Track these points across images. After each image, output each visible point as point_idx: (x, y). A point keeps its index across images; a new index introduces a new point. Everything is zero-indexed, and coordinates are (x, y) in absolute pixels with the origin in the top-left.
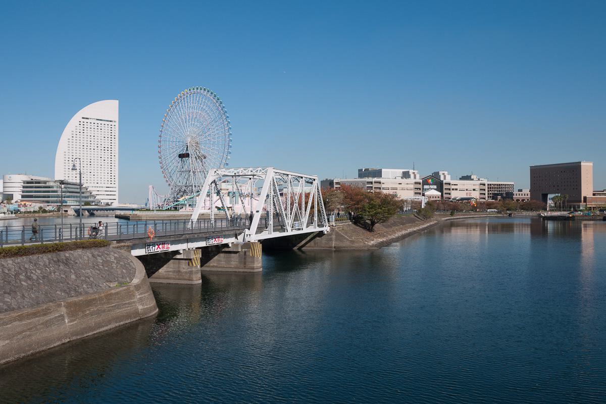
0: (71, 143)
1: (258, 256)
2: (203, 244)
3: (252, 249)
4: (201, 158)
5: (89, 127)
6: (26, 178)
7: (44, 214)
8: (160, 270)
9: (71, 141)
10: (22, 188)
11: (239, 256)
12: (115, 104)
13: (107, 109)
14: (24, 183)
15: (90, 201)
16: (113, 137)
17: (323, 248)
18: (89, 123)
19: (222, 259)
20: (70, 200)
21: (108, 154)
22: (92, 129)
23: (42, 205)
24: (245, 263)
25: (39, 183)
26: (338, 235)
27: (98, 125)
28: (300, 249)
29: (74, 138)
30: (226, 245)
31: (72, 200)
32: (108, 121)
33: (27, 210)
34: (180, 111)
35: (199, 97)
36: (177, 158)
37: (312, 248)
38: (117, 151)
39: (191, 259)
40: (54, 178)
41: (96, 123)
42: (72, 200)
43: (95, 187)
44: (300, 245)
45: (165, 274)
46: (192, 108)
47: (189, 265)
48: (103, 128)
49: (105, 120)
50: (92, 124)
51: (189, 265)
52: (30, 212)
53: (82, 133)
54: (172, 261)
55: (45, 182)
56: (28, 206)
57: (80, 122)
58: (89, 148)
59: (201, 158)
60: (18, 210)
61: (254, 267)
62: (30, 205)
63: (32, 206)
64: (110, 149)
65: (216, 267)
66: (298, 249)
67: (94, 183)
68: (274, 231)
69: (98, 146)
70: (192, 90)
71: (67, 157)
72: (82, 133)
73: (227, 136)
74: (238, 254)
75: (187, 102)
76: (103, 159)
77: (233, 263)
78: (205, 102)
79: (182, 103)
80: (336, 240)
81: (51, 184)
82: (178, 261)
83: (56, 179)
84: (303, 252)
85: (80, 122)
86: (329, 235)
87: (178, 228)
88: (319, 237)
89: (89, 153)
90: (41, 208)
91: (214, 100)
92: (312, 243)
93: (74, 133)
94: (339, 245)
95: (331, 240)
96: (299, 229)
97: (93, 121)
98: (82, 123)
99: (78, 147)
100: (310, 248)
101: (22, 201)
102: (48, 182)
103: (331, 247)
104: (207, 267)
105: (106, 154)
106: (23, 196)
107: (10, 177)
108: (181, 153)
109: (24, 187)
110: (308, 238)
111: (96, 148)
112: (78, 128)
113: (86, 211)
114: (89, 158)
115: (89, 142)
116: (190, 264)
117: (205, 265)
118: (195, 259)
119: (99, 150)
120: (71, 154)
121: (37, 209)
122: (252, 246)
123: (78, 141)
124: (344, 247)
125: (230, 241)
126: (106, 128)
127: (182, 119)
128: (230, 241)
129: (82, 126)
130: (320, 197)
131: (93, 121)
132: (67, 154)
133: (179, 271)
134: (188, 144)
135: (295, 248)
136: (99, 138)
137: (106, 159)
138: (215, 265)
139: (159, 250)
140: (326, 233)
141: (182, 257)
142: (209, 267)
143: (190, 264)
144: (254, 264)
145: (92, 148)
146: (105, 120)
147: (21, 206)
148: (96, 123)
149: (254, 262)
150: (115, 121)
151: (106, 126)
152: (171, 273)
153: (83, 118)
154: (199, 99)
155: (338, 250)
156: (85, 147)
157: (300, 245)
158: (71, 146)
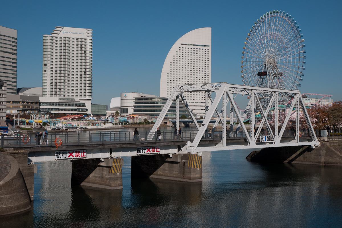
0: (172, 66)
1: (196, 167)
2: (135, 153)
3: (190, 160)
4: (278, 75)
5: (187, 51)
6: (137, 96)
7: (147, 125)
8: (90, 176)
9: (172, 64)
10: (134, 104)
11: (180, 166)
12: (90, 31)
13: (202, 36)
14: (136, 100)
15: (187, 115)
16: (207, 59)
17: (312, 163)
18: (187, 48)
19: (167, 168)
20: (170, 114)
21: (202, 74)
22: (190, 54)
23: (146, 117)
24: (184, 173)
25: (147, 99)
26: (328, 150)
27: (194, 50)
28: (290, 163)
29: (175, 62)
30: (167, 156)
31: (172, 114)
32: (202, 46)
33: (134, 121)
34: (260, 34)
35: (276, 20)
36: (257, 77)
37: (302, 163)
38: (210, 72)
39: (110, 167)
40: (159, 96)
41: (193, 48)
42: (172, 114)
43: (192, 103)
44: (291, 158)
45: (93, 179)
46: (270, 30)
47: (109, 172)
48: (198, 52)
49: (200, 46)
50: (190, 49)
51: (109, 172)
52: (137, 123)
53: (181, 57)
54: (98, 168)
55: (151, 99)
56: (135, 118)
57: (180, 48)
58: (187, 69)
59: (278, 75)
60: (127, 121)
61: (191, 177)
62: (137, 118)
63: (138, 118)
64: (204, 70)
65: (162, 175)
66: (288, 163)
67: (191, 99)
68: (227, 145)
69: (194, 67)
70: (269, 14)
71: (169, 77)
72: (181, 57)
73: (301, 54)
74: (179, 164)
75: (266, 25)
76: (198, 78)
77: (174, 172)
78: (281, 24)
79: (261, 27)
80: (326, 155)
81: (156, 100)
82: (102, 168)
83: (160, 97)
84: (292, 166)
85: (180, 48)
86: (318, 149)
87: (103, 138)
88: (309, 151)
89: (187, 74)
90: (145, 120)
91: (289, 22)
92: (302, 157)
93: (175, 57)
94: (329, 161)
95: (320, 154)
96: (272, 143)
97: (190, 47)
98: (181, 49)
99: (178, 69)
100: (299, 163)
101: (134, 114)
102: (154, 98)
103: (320, 162)
104: (155, 175)
105: (201, 74)
106: (135, 111)
107: (126, 95)
108: (260, 71)
109: (136, 103)
110: (298, 152)
111: (193, 69)
112: (178, 53)
113: (182, 123)
114: (187, 78)
115: (187, 64)
116: (110, 171)
117: (154, 173)
118: (114, 167)
119: (195, 71)
120: (172, 75)
121: (142, 120)
122: (189, 158)
123: (178, 64)
124: (334, 163)
125: (171, 152)
126: (201, 52)
127: (261, 41)
128: (171, 152)
129: (181, 51)
130: (305, 114)
131: (190, 47)
132: (169, 75)
133: (102, 177)
134: (267, 63)
135: (286, 161)
136: (195, 61)
137: (201, 79)
138: (161, 173)
139: (71, 157)
140: (314, 147)
141: (104, 165)
142: (157, 175)
143: (110, 171)
144: (191, 175)
145: (190, 69)
146: (200, 46)
147: (130, 118)
148: (181, 48)
149: (191, 173)
150: (208, 46)
151: (201, 50)
152: (97, 179)
153: (182, 44)
154: (276, 22)
155: (327, 165)
156: (184, 69)
157: (291, 158)
158: (172, 68)
